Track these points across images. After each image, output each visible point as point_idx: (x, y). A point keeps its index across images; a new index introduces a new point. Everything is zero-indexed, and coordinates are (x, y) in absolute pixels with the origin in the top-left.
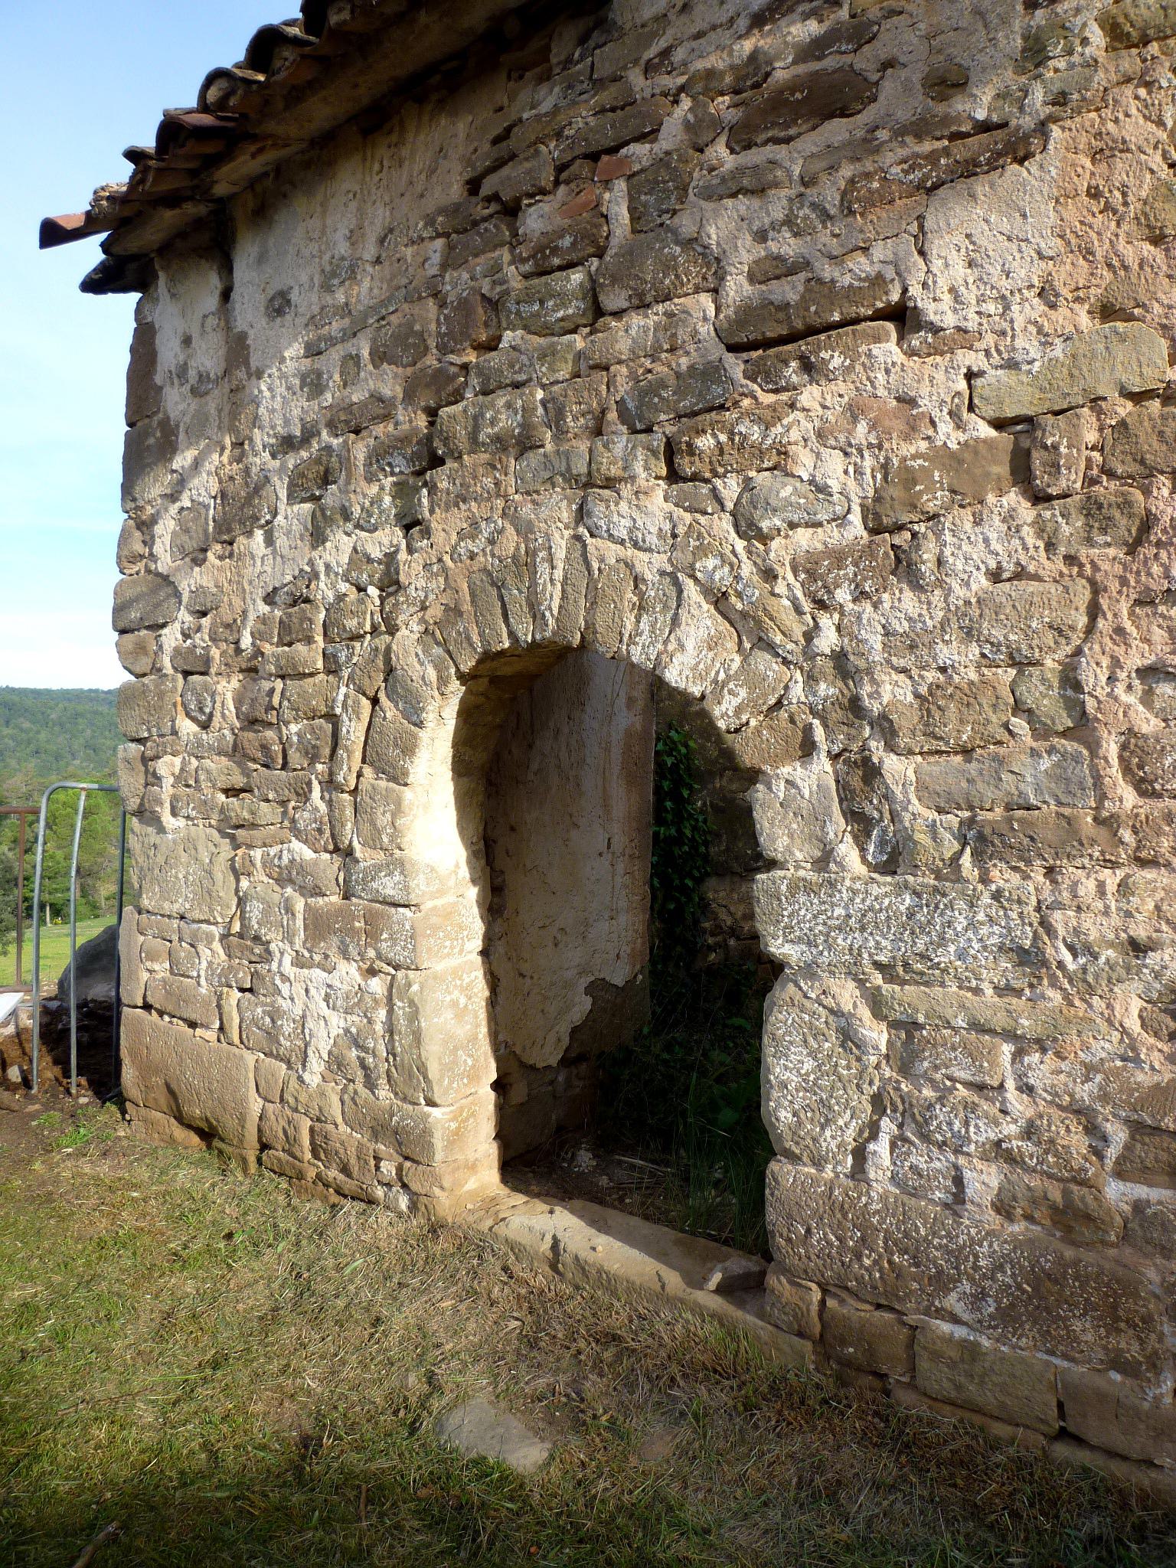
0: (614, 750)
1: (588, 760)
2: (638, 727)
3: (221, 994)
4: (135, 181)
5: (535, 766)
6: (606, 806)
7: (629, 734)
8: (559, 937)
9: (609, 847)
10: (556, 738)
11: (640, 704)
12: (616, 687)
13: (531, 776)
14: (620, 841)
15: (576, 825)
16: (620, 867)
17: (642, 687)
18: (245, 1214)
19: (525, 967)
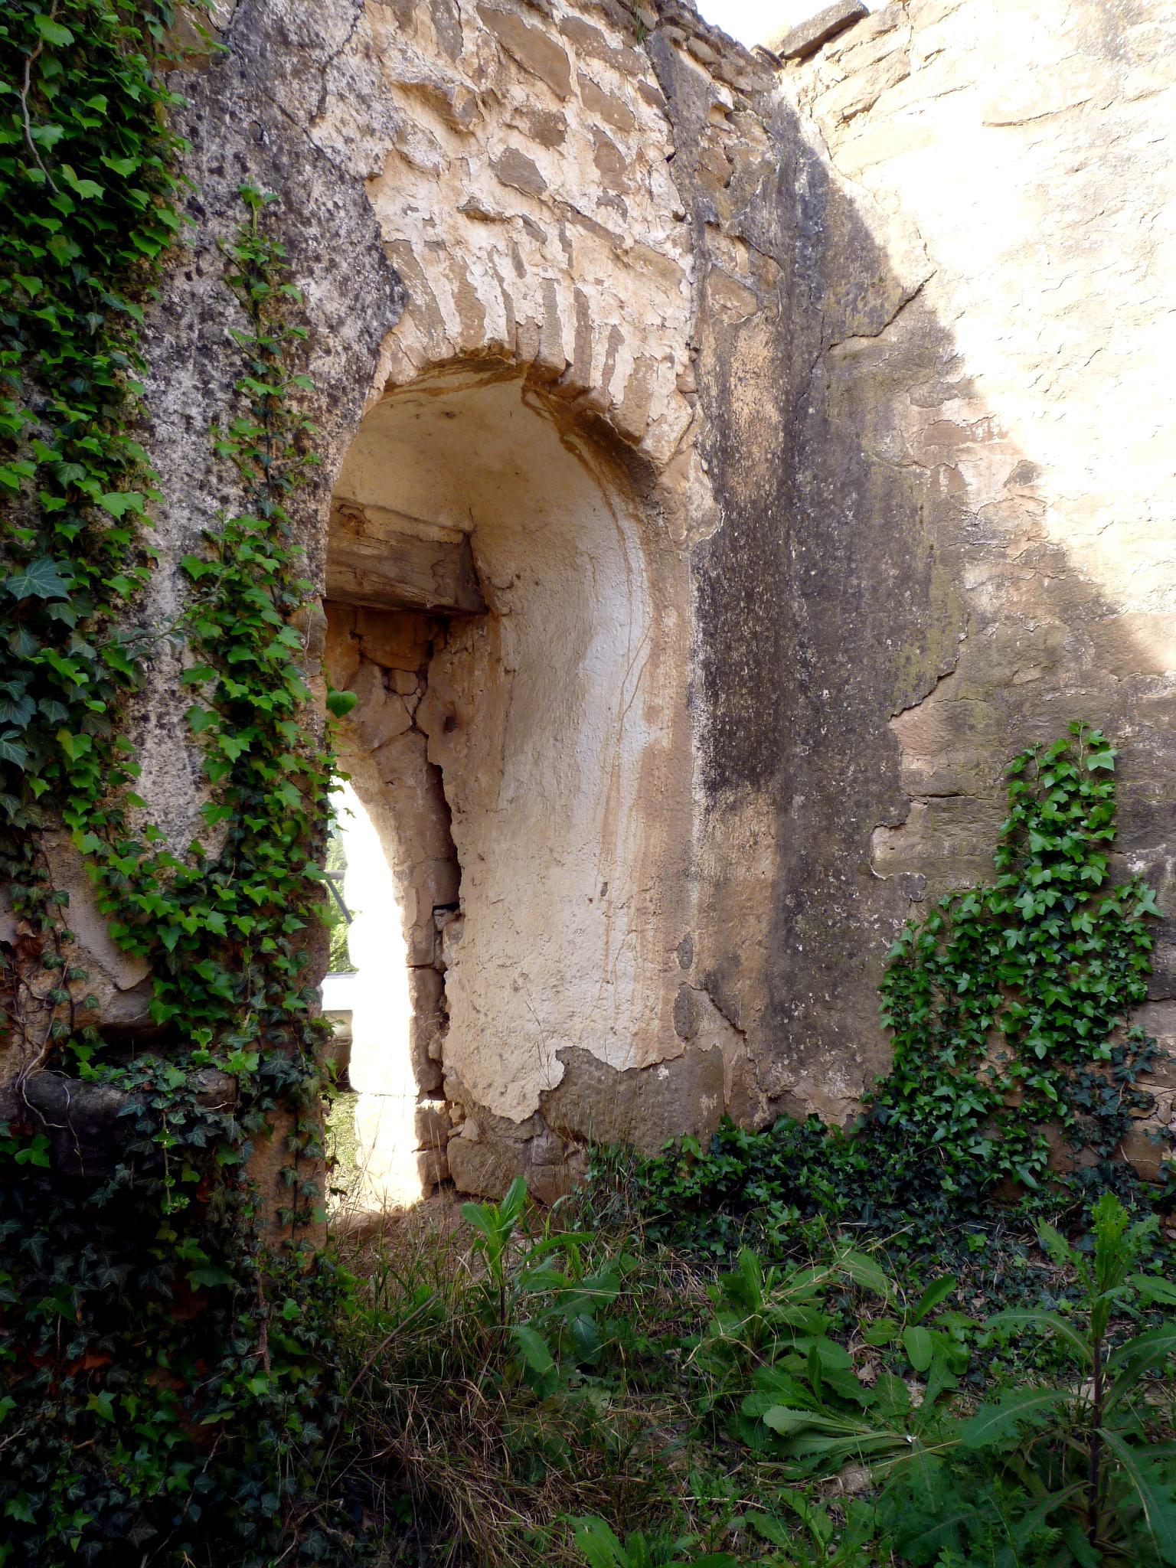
0: (625, 775)
1: (584, 787)
2: (666, 743)
3: (266, 88)
4: (323, 1121)
5: (510, 793)
6: (607, 835)
7: (650, 754)
8: (520, 981)
9: (603, 893)
10: (536, 762)
11: (668, 714)
12: (627, 698)
13: (503, 804)
14: (623, 887)
15: (559, 863)
16: (622, 921)
17: (671, 691)
18: (357, 298)
19: (480, 1002)
